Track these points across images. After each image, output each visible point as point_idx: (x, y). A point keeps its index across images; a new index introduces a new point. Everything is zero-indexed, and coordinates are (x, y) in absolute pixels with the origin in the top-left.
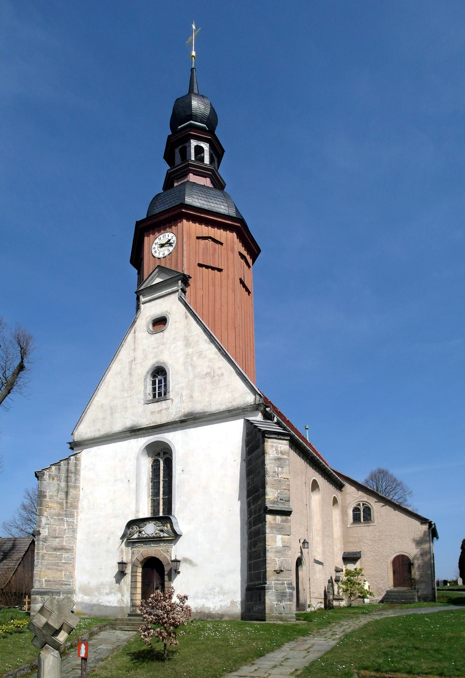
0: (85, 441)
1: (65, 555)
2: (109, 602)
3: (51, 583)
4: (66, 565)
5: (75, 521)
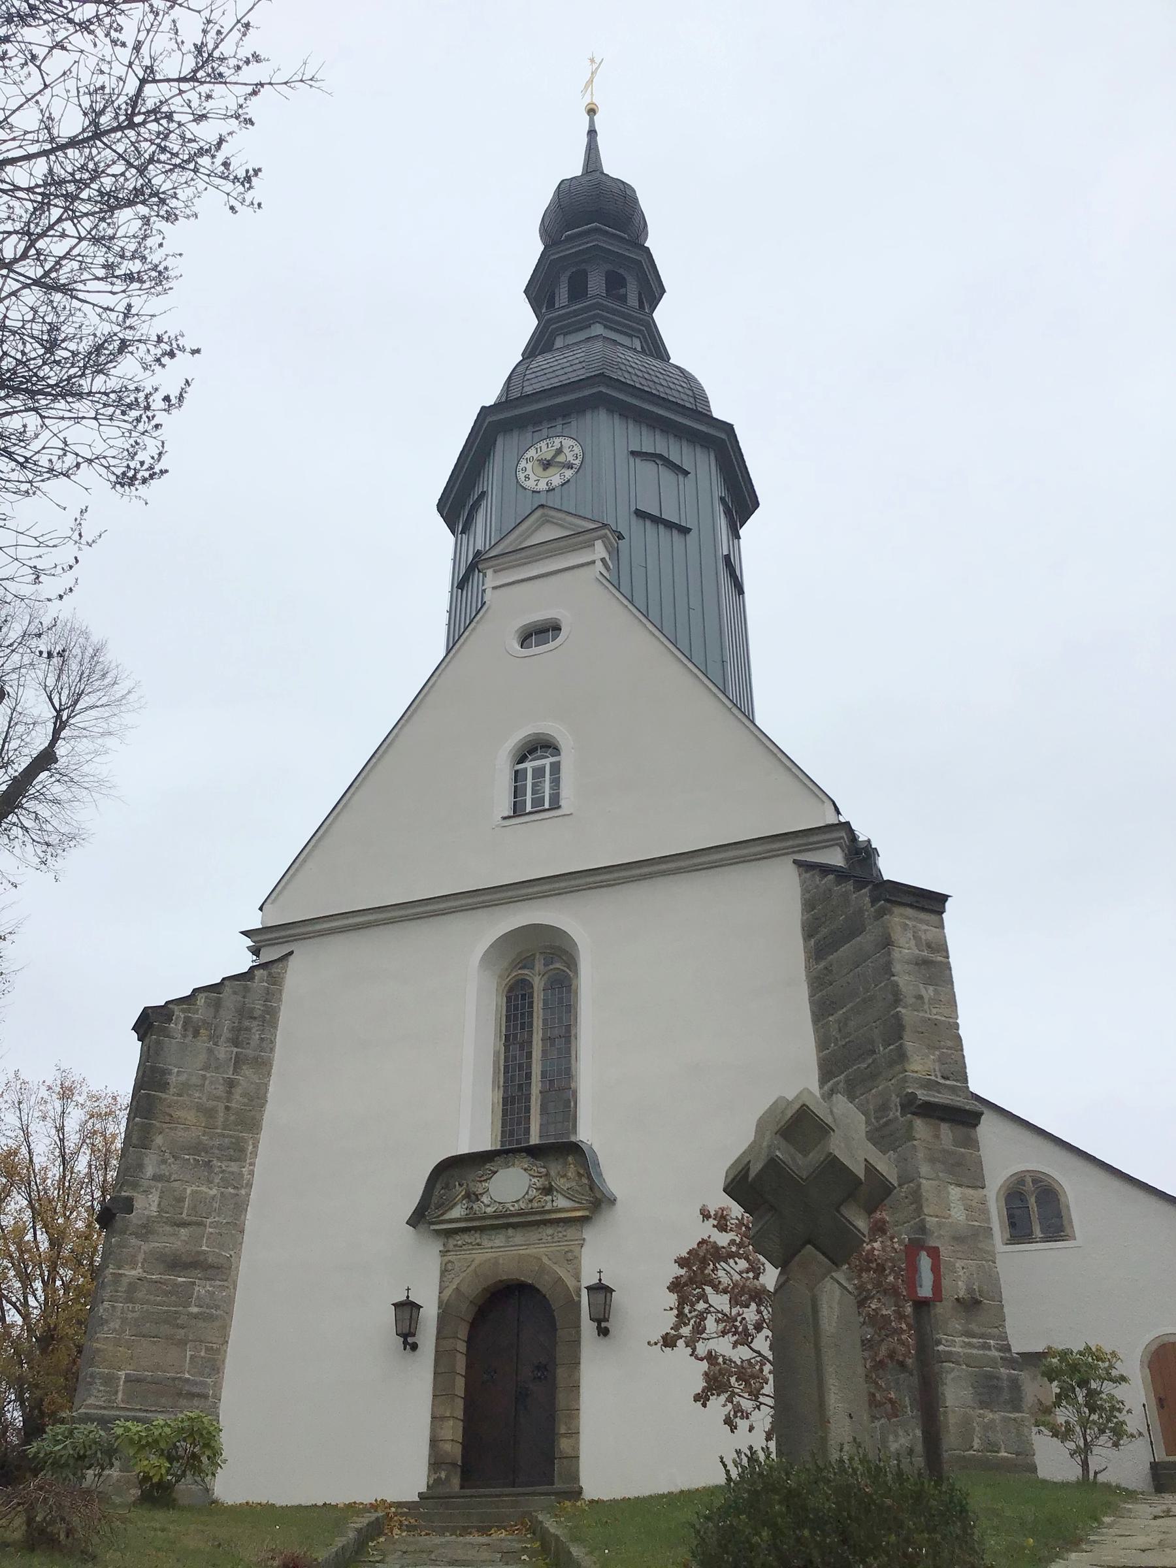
1: (202, 1289)
4: (201, 1324)
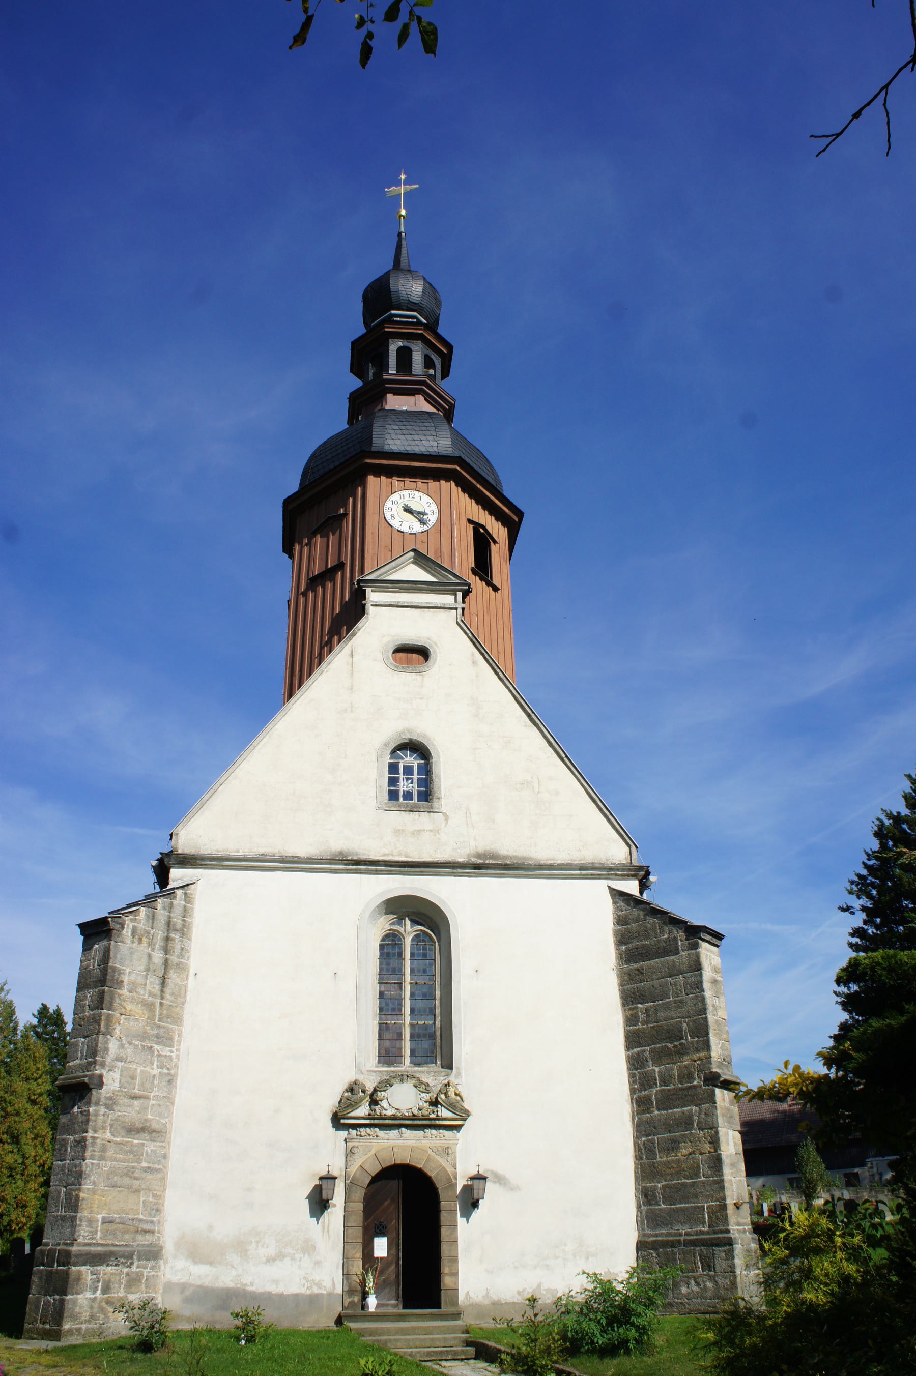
0: (204, 858)
1: (150, 1147)
2: (276, 1282)
3: (114, 1226)
4: (149, 1176)
5: (174, 1055)
